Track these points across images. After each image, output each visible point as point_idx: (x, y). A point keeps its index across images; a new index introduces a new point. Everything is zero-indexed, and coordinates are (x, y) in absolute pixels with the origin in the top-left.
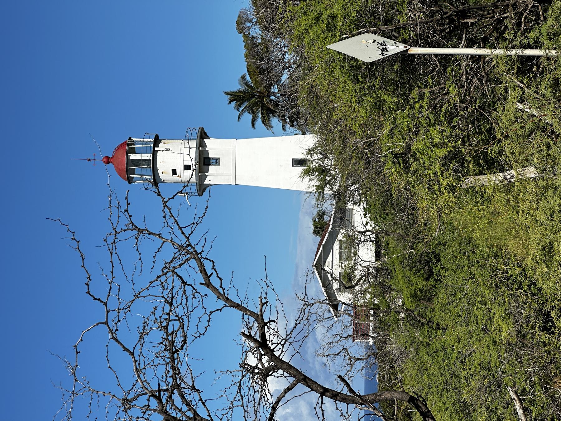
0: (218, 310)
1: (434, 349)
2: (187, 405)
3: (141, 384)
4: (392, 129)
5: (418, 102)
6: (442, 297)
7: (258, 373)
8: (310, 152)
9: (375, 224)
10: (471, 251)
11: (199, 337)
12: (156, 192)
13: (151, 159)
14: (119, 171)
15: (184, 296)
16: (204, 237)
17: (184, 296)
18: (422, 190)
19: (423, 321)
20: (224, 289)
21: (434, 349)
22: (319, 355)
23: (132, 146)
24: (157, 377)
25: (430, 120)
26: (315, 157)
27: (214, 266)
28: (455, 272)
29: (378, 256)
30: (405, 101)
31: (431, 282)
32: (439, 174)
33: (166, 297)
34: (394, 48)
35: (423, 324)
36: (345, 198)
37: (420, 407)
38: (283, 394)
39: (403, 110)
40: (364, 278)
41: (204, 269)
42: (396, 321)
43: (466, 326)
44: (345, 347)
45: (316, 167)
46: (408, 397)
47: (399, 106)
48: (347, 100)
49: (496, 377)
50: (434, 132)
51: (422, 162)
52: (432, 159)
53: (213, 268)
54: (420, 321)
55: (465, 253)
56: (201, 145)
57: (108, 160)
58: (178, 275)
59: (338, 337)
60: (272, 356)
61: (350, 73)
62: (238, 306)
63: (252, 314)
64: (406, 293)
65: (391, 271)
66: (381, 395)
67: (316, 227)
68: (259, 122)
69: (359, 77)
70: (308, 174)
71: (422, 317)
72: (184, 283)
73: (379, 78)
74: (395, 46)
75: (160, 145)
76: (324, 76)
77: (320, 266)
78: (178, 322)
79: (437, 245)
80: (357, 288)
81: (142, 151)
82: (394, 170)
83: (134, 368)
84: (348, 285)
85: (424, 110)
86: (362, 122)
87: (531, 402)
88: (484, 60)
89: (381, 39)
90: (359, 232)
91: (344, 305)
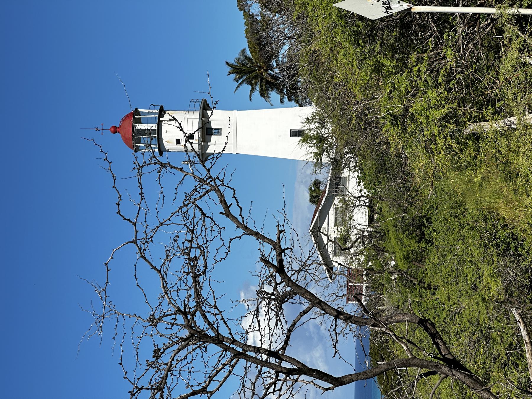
0: (237, 237)
1: (425, 307)
2: (209, 324)
3: (168, 300)
4: (391, 92)
5: (416, 66)
6: (434, 257)
7: (274, 299)
8: (308, 121)
9: (368, 192)
10: (461, 214)
11: (221, 261)
12: (178, 128)
13: (156, 128)
14: (126, 141)
16: (224, 171)
18: (420, 150)
19: (415, 281)
20: (243, 218)
21: (425, 307)
22: (316, 313)
23: (139, 117)
24: (182, 296)
26: (313, 126)
27: (234, 194)
28: (446, 235)
29: (371, 219)
31: (423, 245)
32: (436, 134)
35: (414, 284)
37: (429, 328)
38: (299, 318)
39: (402, 74)
40: (359, 240)
41: (225, 200)
42: (389, 281)
44: (340, 306)
45: (314, 135)
47: (398, 70)
48: (348, 64)
49: (484, 332)
50: (432, 94)
51: (419, 123)
53: (234, 197)
54: (411, 281)
57: (115, 130)
58: (198, 207)
59: (334, 296)
60: (288, 281)
61: (351, 38)
62: (256, 234)
63: (270, 241)
64: (399, 254)
65: (385, 234)
68: (257, 93)
69: (360, 42)
70: (307, 142)
72: (204, 214)
73: (379, 43)
74: (399, 5)
76: (327, 40)
77: (316, 231)
79: (429, 209)
80: (352, 250)
83: (162, 285)
84: (343, 247)
85: (422, 74)
86: (362, 85)
87: (518, 356)
88: (479, 26)
90: (355, 197)
91: (339, 266)
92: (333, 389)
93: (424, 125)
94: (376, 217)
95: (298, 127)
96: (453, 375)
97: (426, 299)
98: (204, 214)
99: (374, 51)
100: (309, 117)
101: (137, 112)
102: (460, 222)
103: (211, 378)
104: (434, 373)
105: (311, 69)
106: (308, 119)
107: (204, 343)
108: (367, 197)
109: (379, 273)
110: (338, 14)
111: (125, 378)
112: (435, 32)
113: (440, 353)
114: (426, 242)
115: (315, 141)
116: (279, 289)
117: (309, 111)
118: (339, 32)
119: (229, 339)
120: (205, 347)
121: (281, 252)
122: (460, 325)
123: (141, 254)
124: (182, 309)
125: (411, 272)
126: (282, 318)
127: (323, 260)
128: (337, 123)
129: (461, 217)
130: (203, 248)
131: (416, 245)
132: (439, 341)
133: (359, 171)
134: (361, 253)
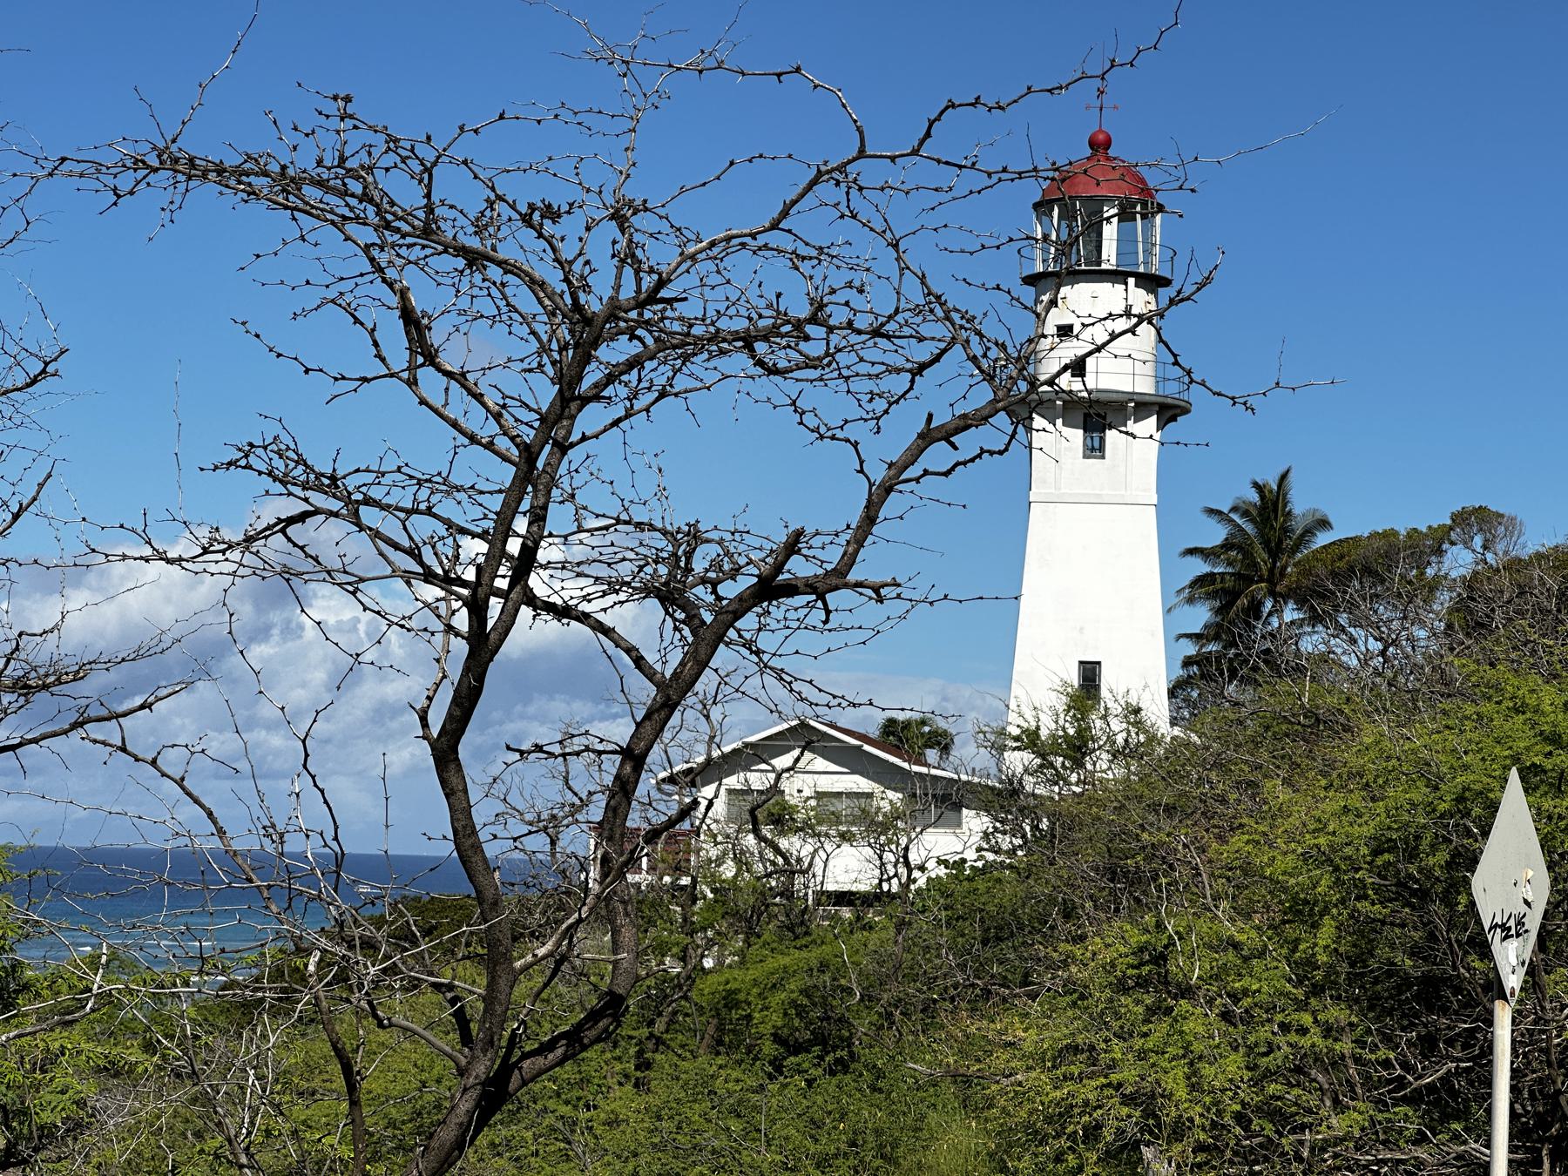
0: (861, 462)
4: (1236, 946)
5: (1316, 1021)
6: (733, 1079)
12: (1179, 292)
13: (1104, 266)
15: (884, 368)
17: (884, 368)
18: (1064, 1028)
19: (660, 1025)
20: (917, 480)
24: (697, 300)
25: (1266, 1054)
26: (1116, 725)
27: (992, 453)
28: (799, 1116)
29: (843, 898)
30: (1313, 983)
31: (769, 1048)
32: (1114, 1078)
33: (899, 318)
34: (1511, 959)
35: (651, 1023)
36: (1002, 807)
39: (1289, 980)
40: (780, 860)
41: (969, 426)
42: (661, 949)
43: (654, 1146)
46: (621, 991)
48: (1319, 820)
50: (1234, 1064)
51: (1145, 1029)
52: (1153, 1058)
53: (983, 451)
54: (660, 1014)
55: (853, 1144)
56: (1143, 407)
57: (1100, 145)
58: (944, 351)
62: (870, 517)
63: (849, 561)
66: (627, 914)
67: (907, 725)
68: (1200, 567)
69: (1386, 856)
70: (1069, 708)
71: (671, 1022)
72: (922, 367)
74: (1514, 962)
75: (1142, 292)
76: (1389, 758)
77: (805, 737)
78: (822, 352)
79: (875, 1066)
80: (750, 840)
81: (1125, 241)
82: (1122, 949)
83: (734, 232)
84: (760, 814)
85: (1293, 1037)
89: (1534, 922)
90: (907, 849)
92: (424, 738)
93: (1138, 1043)
94: (846, 913)
95: (1109, 681)
96: (465, 1090)
97: (608, 1055)
98: (922, 367)
99: (1358, 898)
100: (1143, 713)
101: (1152, 208)
102: (836, 1156)
103: (460, 378)
104: (466, 1039)
105: (1294, 715)
106: (1137, 711)
107: (554, 363)
108: (905, 887)
109: (685, 920)
110: (1468, 789)
111: (462, 128)
112: (1416, 1079)
113: (525, 1056)
114: (776, 1058)
115: (1071, 731)
116: (700, 591)
117: (1158, 711)
118: (1416, 796)
119: (569, 433)
120: (540, 366)
121: (819, 589)
122: (537, 1154)
123: (828, 172)
124: (664, 294)
125: (687, 1015)
126: (612, 598)
127: (724, 756)
128: (1128, 795)
129: (852, 1162)
130: (829, 365)
131: (766, 1029)
132: (560, 1052)
133: (980, 864)
134: (741, 861)
